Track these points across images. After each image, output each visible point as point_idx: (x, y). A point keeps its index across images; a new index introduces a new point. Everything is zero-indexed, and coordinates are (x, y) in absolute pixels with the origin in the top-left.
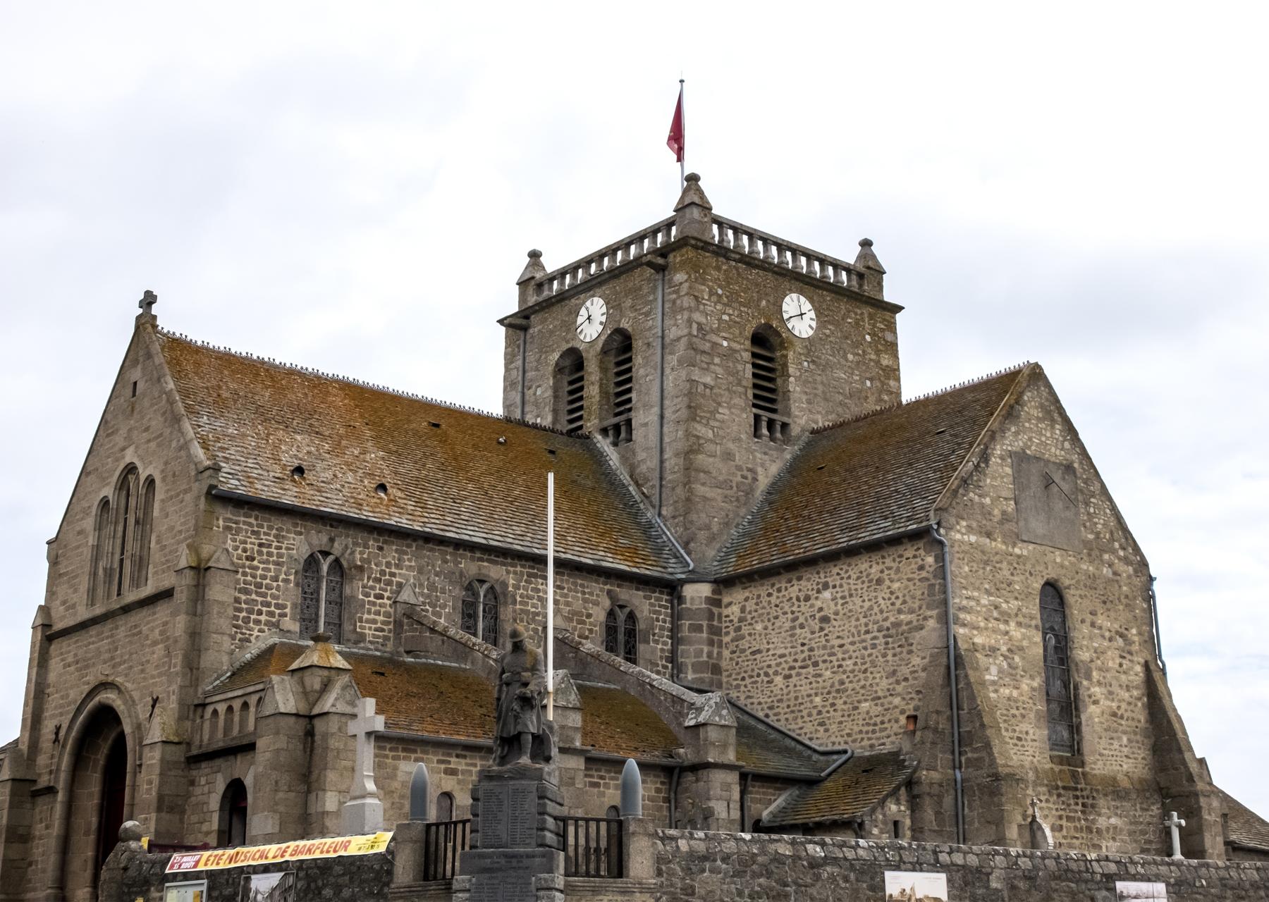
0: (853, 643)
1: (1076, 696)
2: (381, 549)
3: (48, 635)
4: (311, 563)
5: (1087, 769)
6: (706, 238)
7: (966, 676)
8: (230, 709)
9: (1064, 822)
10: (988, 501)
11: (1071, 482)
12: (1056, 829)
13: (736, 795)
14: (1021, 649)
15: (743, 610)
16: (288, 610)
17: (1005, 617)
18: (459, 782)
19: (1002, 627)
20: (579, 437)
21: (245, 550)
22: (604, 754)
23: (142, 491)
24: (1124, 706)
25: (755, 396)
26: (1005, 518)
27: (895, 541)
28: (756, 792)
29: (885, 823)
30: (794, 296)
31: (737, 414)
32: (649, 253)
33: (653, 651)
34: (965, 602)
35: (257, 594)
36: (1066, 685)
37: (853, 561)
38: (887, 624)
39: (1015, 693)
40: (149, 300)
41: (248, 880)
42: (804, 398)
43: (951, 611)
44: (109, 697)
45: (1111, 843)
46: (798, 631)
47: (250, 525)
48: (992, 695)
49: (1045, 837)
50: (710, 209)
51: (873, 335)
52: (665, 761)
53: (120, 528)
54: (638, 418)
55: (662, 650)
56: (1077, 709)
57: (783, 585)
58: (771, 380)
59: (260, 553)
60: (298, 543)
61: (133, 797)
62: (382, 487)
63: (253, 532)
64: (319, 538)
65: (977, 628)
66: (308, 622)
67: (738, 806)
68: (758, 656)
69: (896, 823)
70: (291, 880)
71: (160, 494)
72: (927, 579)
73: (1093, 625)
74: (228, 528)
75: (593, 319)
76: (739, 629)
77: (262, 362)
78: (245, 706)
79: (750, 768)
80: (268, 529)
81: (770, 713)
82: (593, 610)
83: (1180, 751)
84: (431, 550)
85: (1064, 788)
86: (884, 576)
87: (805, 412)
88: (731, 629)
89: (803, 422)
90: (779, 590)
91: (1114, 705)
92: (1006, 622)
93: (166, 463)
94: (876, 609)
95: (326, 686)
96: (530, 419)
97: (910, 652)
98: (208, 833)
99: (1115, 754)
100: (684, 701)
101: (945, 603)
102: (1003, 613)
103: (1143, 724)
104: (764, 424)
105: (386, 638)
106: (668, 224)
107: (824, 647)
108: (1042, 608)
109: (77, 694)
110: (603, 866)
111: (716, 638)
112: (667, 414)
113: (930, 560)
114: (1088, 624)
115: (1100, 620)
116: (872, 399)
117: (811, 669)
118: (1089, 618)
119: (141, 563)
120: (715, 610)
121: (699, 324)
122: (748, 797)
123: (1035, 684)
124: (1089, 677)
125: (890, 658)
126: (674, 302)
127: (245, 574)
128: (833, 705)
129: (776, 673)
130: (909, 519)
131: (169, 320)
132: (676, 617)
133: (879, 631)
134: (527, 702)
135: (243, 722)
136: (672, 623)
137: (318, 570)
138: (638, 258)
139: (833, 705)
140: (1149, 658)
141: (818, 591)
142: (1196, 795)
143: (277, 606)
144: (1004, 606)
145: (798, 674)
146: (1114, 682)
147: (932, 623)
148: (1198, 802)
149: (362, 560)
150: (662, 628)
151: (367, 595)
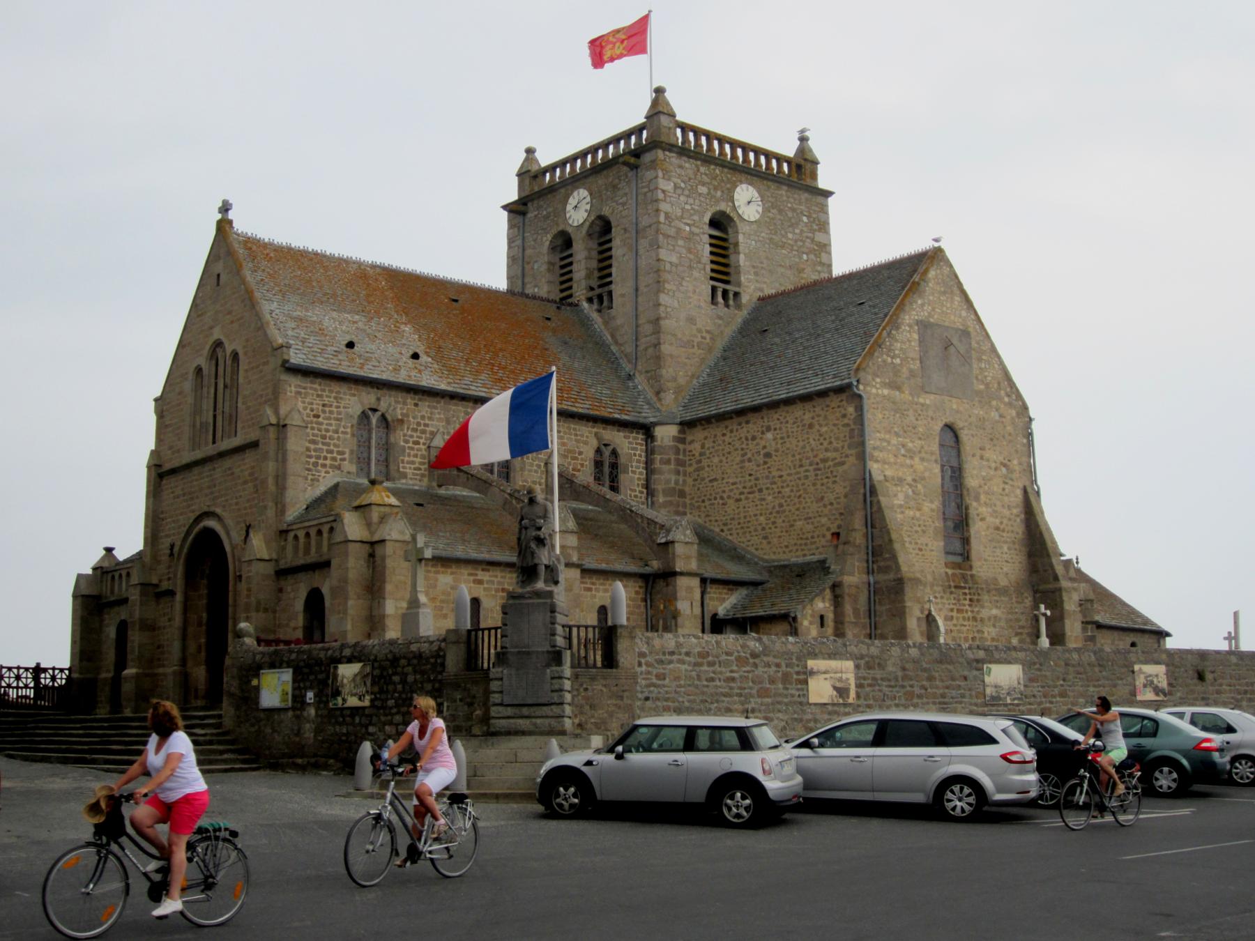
0: (789, 475)
1: (967, 515)
2: (416, 405)
3: (161, 474)
4: (364, 416)
5: (974, 572)
6: (672, 141)
7: (879, 502)
8: (308, 535)
9: (955, 614)
10: (898, 361)
11: (963, 348)
12: (948, 619)
13: (697, 595)
14: (923, 478)
15: (703, 447)
16: (347, 456)
17: (911, 454)
18: (485, 589)
19: (908, 462)
20: (571, 305)
21: (312, 410)
22: (594, 566)
23: (229, 362)
24: (1005, 521)
25: (712, 270)
26: (912, 374)
27: (822, 394)
28: (713, 591)
29: (812, 616)
30: (744, 186)
31: (699, 284)
32: (624, 154)
33: (632, 480)
34: (878, 443)
35: (323, 444)
36: (959, 507)
37: (791, 408)
38: (817, 460)
39: (918, 514)
40: (225, 208)
41: (336, 668)
42: (752, 271)
43: (868, 450)
44: (211, 523)
45: (991, 629)
46: (747, 464)
47: (316, 390)
48: (899, 516)
49: (938, 628)
50: (674, 116)
51: (808, 217)
52: (642, 570)
53: (212, 391)
54: (617, 289)
55: (639, 479)
56: (967, 525)
57: (735, 427)
58: (727, 274)
59: (324, 412)
60: (354, 402)
61: (235, 601)
62: (415, 356)
63: (318, 396)
64: (368, 397)
65: (889, 463)
66: (363, 462)
67: (699, 604)
68: (715, 484)
69: (822, 617)
70: (368, 669)
71: (243, 366)
72: (848, 425)
73: (982, 458)
74: (298, 393)
75: (578, 210)
76: (699, 462)
77: (316, 254)
78: (320, 533)
79: (710, 573)
80: (330, 392)
81: (725, 528)
82: (584, 448)
83: (1048, 555)
84: (456, 405)
85: (956, 587)
86: (814, 421)
87: (754, 283)
88: (693, 462)
89: (751, 290)
90: (731, 431)
91: (997, 521)
92: (911, 458)
93: (247, 340)
94: (808, 448)
95: (383, 519)
96: (529, 290)
97: (835, 482)
98: (295, 629)
99: (997, 558)
100: (656, 523)
101: (863, 444)
102: (909, 451)
103: (1020, 536)
104: (719, 294)
105: (423, 475)
106: (638, 130)
107: (767, 477)
108: (941, 445)
109: (187, 519)
110: (599, 658)
111: (681, 469)
112: (642, 288)
113: (851, 409)
114: (978, 457)
115: (987, 454)
116: (808, 270)
117: (757, 494)
118: (979, 453)
119: (233, 418)
120: (681, 446)
121: (666, 214)
122: (707, 596)
123: (934, 506)
124: (977, 499)
125: (819, 486)
126: (645, 194)
127: (313, 428)
128: (774, 523)
129: (729, 497)
130: (835, 376)
131: (243, 223)
132: (650, 452)
133: (811, 465)
134: (541, 542)
135: (319, 545)
136: (647, 457)
137: (369, 422)
138: (616, 158)
139: (774, 523)
140: (1027, 484)
141: (763, 433)
142: (1060, 589)
143: (339, 453)
144: (910, 445)
145: (747, 498)
146: (998, 503)
147: (852, 460)
148: (1061, 597)
149: (402, 414)
150: (638, 461)
151: (406, 442)
